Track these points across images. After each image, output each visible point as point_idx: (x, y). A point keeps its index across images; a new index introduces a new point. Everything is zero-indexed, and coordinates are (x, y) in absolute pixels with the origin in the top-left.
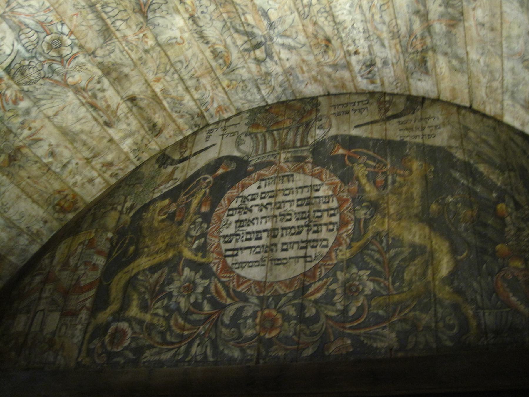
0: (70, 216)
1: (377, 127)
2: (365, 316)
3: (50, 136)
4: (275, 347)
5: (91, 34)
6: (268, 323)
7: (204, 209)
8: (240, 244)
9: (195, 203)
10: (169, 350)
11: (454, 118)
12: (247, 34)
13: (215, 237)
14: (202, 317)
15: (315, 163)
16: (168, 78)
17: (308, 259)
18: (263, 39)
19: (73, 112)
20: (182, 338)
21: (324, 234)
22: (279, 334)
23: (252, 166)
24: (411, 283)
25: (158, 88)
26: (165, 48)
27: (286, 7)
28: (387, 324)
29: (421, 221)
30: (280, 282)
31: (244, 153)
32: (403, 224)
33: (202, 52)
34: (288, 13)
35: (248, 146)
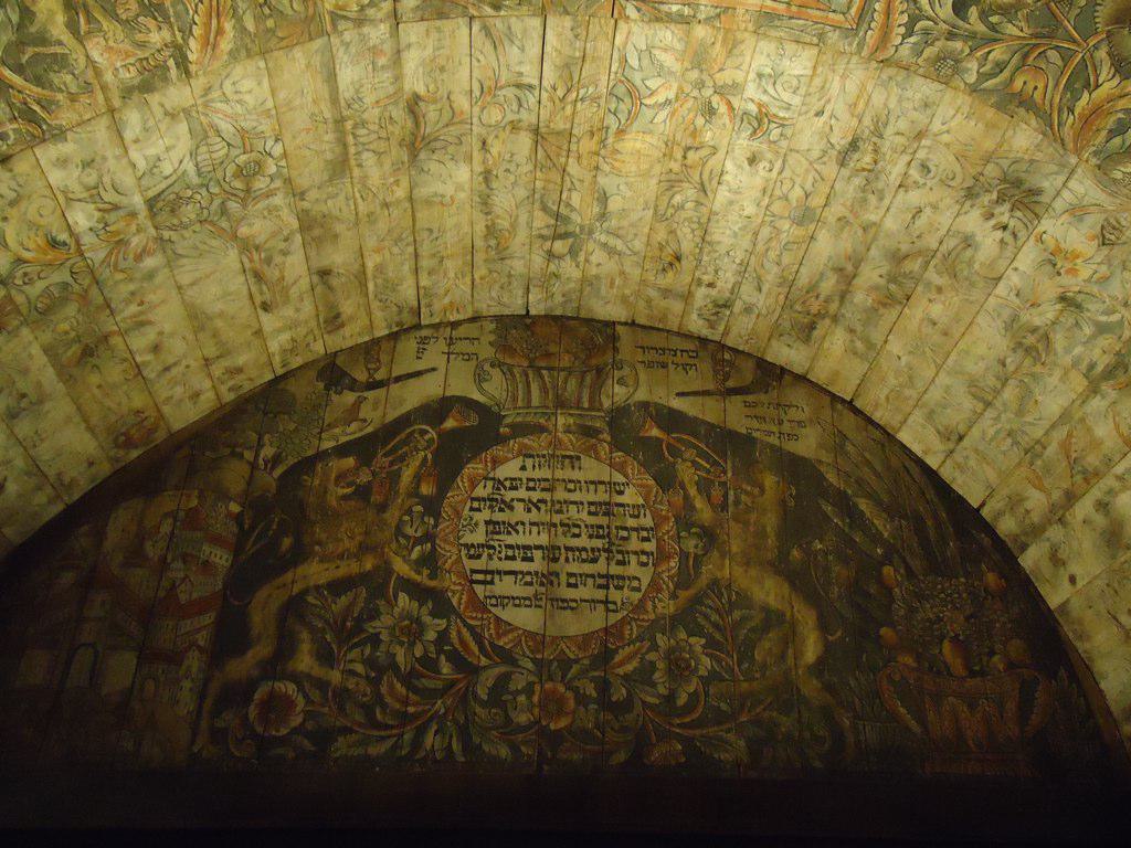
1: (710, 402)
3: (168, 316)
4: (567, 745)
6: (552, 705)
7: (427, 489)
8: (496, 564)
9: (407, 475)
10: (383, 738)
11: (827, 414)
12: (557, 216)
14: (439, 684)
18: (578, 229)
19: (218, 279)
20: (404, 719)
21: (633, 568)
23: (507, 426)
24: (764, 666)
29: (778, 572)
32: (753, 572)
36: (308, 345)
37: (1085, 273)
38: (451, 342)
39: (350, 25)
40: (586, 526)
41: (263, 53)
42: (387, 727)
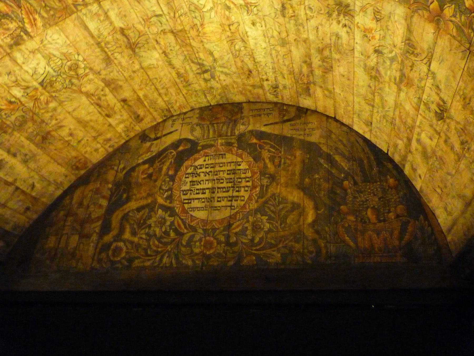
0: (82, 172)
1: (277, 126)
2: (263, 244)
3: (70, 124)
4: (213, 259)
5: (97, 61)
6: (209, 245)
7: (171, 173)
8: (193, 196)
9: (165, 168)
10: (149, 260)
12: (199, 64)
13: (178, 191)
15: (239, 148)
16: (148, 88)
17: (233, 208)
18: (209, 68)
19: (85, 109)
20: (157, 252)
21: (242, 193)
22: (215, 251)
24: (291, 224)
25: (141, 94)
26: (147, 70)
27: (224, 51)
28: (276, 249)
30: (216, 220)
31: (196, 137)
32: (289, 190)
33: (170, 73)
34: (226, 54)
35: (198, 133)
36: (133, 128)
37: (377, 37)
38: (183, 119)
39: (82, 7)
40: (226, 179)
41: (56, 24)
42: (151, 256)
